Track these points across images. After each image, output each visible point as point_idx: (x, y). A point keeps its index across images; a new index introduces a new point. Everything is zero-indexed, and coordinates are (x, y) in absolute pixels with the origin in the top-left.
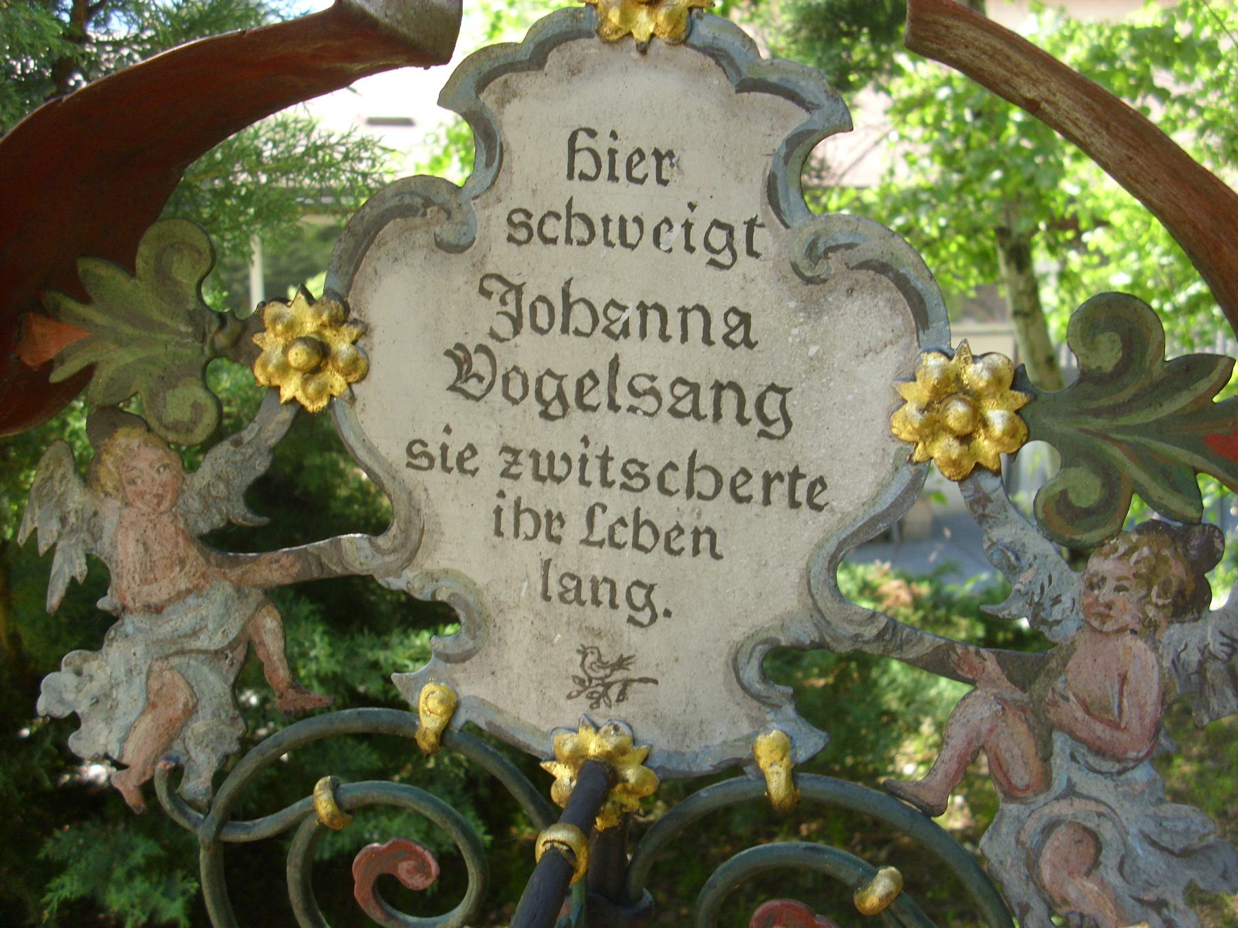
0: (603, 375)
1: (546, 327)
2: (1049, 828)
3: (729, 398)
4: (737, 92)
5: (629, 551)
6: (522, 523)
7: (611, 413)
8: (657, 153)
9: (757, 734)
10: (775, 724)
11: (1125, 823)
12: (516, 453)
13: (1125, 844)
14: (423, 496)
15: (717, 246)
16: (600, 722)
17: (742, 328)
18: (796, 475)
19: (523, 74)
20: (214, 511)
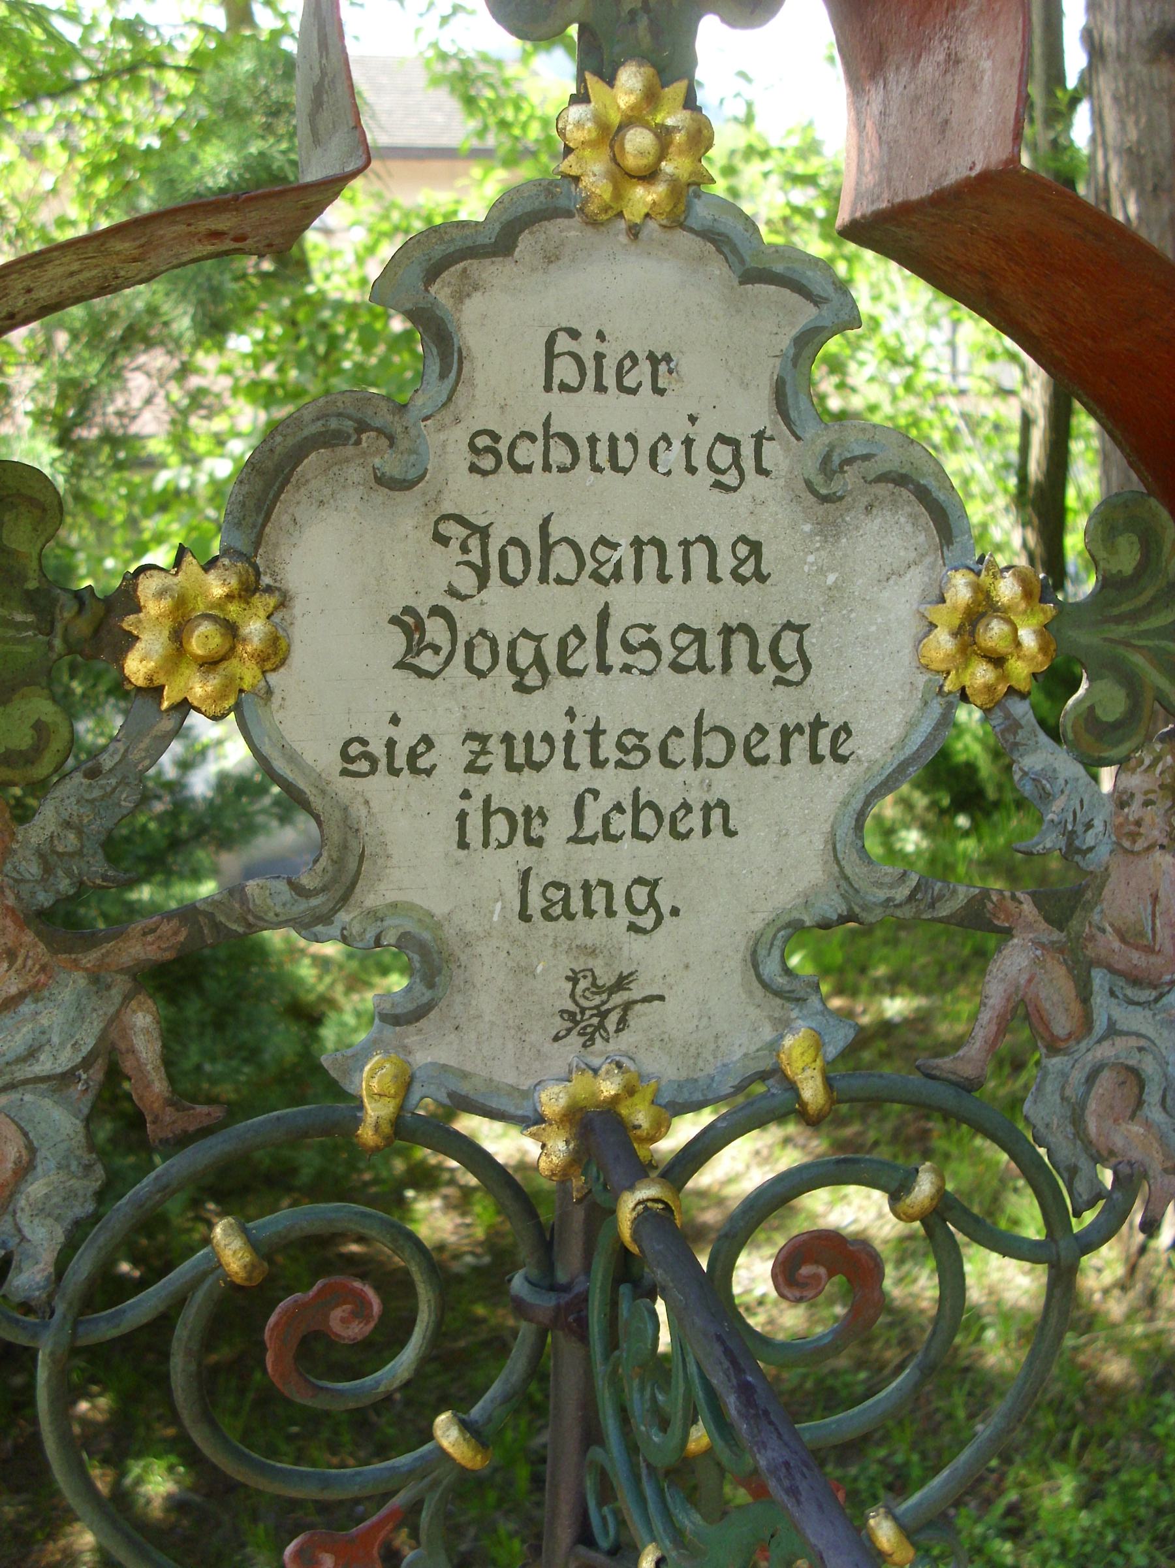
0: (590, 631)
1: (519, 576)
2: (1091, 1078)
3: (740, 643)
4: (741, 283)
5: (627, 843)
6: (492, 828)
7: (601, 676)
8: (651, 357)
9: (782, 1037)
10: (800, 1022)
11: (1165, 1053)
12: (483, 739)
13: (1165, 1075)
14: (363, 812)
15: (722, 466)
16: (596, 1062)
17: (752, 559)
18: (818, 724)
19: (487, 261)
20: (60, 873)
